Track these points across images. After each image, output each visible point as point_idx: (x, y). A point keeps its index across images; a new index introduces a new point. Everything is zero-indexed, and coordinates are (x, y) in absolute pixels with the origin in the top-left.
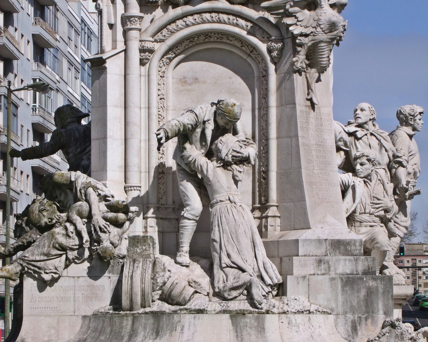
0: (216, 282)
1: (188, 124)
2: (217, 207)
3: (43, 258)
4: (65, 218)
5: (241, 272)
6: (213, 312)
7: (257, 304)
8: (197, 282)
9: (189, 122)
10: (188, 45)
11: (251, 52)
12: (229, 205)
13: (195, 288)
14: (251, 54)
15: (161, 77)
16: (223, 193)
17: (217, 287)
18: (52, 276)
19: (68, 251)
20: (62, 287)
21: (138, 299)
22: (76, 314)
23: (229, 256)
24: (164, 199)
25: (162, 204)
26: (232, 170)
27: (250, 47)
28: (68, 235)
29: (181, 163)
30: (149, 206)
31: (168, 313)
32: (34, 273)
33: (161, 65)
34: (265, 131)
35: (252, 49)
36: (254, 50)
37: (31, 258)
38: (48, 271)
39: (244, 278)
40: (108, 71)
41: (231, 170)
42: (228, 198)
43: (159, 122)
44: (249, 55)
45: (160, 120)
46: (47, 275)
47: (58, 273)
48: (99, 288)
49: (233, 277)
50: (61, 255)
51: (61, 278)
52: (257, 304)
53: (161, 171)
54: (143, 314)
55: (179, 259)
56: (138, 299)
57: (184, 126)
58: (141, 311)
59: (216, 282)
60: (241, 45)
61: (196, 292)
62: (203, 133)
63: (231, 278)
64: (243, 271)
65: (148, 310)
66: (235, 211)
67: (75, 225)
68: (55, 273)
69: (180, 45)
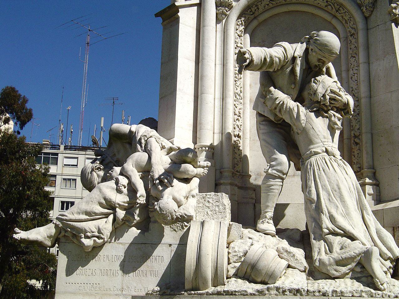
0: (316, 254)
1: (275, 57)
2: (313, 159)
3: (84, 217)
4: (119, 172)
5: (349, 241)
6: (317, 294)
7: (379, 283)
8: (290, 252)
9: (277, 55)
10: (268, 5)
11: (337, 11)
12: (327, 157)
13: (288, 260)
14: (337, 15)
15: (238, 35)
16: (319, 143)
17: (318, 260)
18: (94, 240)
19: (117, 209)
20: (108, 256)
21: (209, 272)
22: (124, 292)
23: (332, 219)
24: (240, 165)
25: (237, 171)
26: (329, 118)
27: (336, 5)
28: (119, 191)
29: (264, 112)
30: (222, 170)
31: (251, 294)
32: (73, 237)
33: (238, 23)
34: (356, 91)
35: (338, 7)
36: (341, 8)
37: (71, 217)
38: (89, 234)
39: (355, 248)
40: (181, 21)
41: (327, 117)
42: (324, 150)
43: (236, 81)
44: (335, 17)
45: (237, 80)
46: (88, 240)
47: (103, 237)
48: (156, 259)
49: (340, 247)
50: (107, 216)
51: (106, 244)
52: (379, 283)
53: (237, 134)
54: (215, 294)
55: (260, 226)
56: (209, 272)
57: (271, 57)
58: (211, 289)
59: (316, 254)
60: (326, 4)
61: (289, 266)
62: (293, 71)
63: (336, 248)
64: (353, 238)
65: (219, 288)
66: (335, 165)
67: (128, 178)
68: (99, 238)
69: (260, 3)
